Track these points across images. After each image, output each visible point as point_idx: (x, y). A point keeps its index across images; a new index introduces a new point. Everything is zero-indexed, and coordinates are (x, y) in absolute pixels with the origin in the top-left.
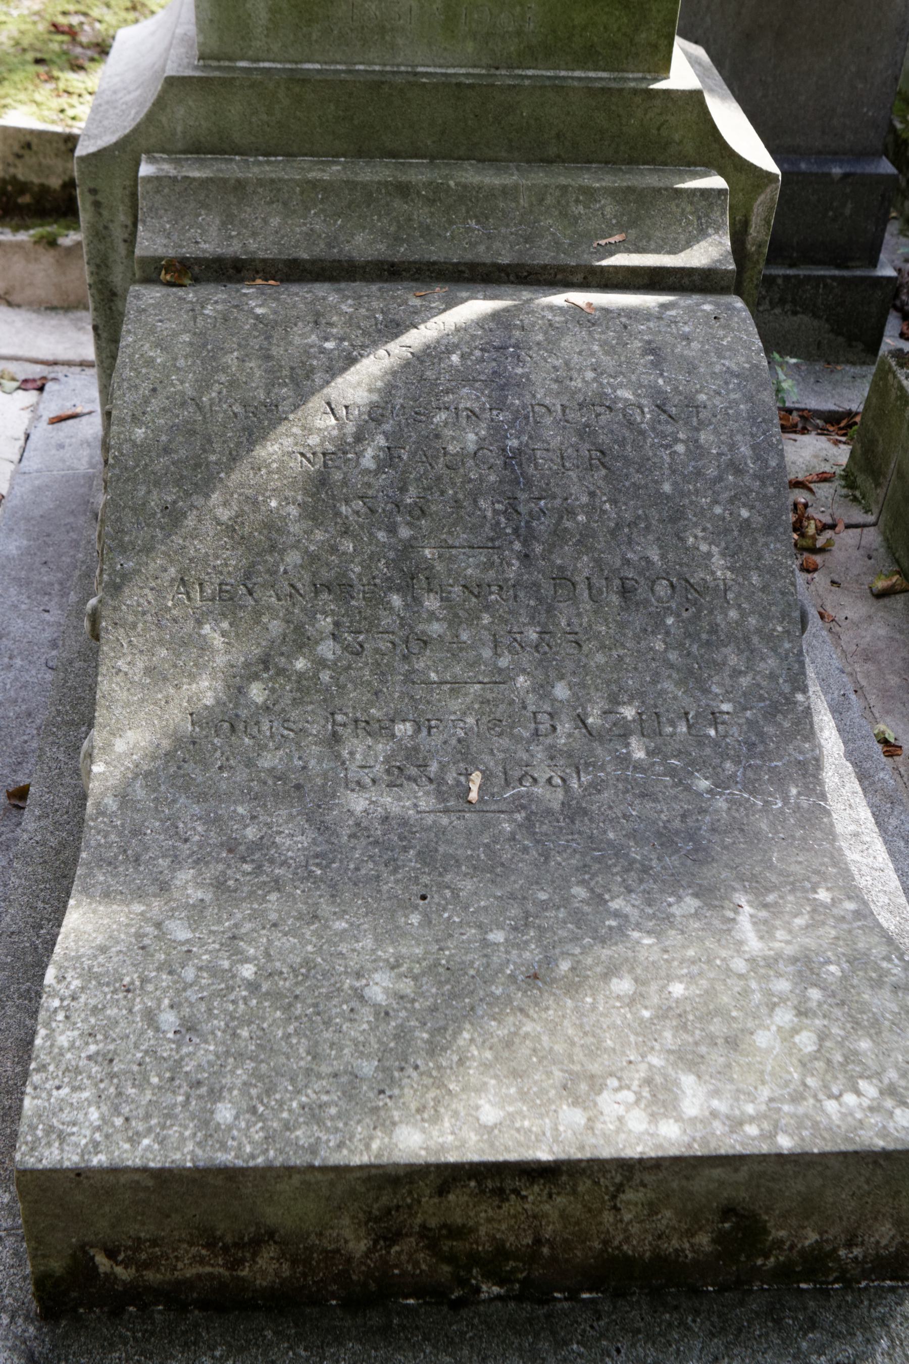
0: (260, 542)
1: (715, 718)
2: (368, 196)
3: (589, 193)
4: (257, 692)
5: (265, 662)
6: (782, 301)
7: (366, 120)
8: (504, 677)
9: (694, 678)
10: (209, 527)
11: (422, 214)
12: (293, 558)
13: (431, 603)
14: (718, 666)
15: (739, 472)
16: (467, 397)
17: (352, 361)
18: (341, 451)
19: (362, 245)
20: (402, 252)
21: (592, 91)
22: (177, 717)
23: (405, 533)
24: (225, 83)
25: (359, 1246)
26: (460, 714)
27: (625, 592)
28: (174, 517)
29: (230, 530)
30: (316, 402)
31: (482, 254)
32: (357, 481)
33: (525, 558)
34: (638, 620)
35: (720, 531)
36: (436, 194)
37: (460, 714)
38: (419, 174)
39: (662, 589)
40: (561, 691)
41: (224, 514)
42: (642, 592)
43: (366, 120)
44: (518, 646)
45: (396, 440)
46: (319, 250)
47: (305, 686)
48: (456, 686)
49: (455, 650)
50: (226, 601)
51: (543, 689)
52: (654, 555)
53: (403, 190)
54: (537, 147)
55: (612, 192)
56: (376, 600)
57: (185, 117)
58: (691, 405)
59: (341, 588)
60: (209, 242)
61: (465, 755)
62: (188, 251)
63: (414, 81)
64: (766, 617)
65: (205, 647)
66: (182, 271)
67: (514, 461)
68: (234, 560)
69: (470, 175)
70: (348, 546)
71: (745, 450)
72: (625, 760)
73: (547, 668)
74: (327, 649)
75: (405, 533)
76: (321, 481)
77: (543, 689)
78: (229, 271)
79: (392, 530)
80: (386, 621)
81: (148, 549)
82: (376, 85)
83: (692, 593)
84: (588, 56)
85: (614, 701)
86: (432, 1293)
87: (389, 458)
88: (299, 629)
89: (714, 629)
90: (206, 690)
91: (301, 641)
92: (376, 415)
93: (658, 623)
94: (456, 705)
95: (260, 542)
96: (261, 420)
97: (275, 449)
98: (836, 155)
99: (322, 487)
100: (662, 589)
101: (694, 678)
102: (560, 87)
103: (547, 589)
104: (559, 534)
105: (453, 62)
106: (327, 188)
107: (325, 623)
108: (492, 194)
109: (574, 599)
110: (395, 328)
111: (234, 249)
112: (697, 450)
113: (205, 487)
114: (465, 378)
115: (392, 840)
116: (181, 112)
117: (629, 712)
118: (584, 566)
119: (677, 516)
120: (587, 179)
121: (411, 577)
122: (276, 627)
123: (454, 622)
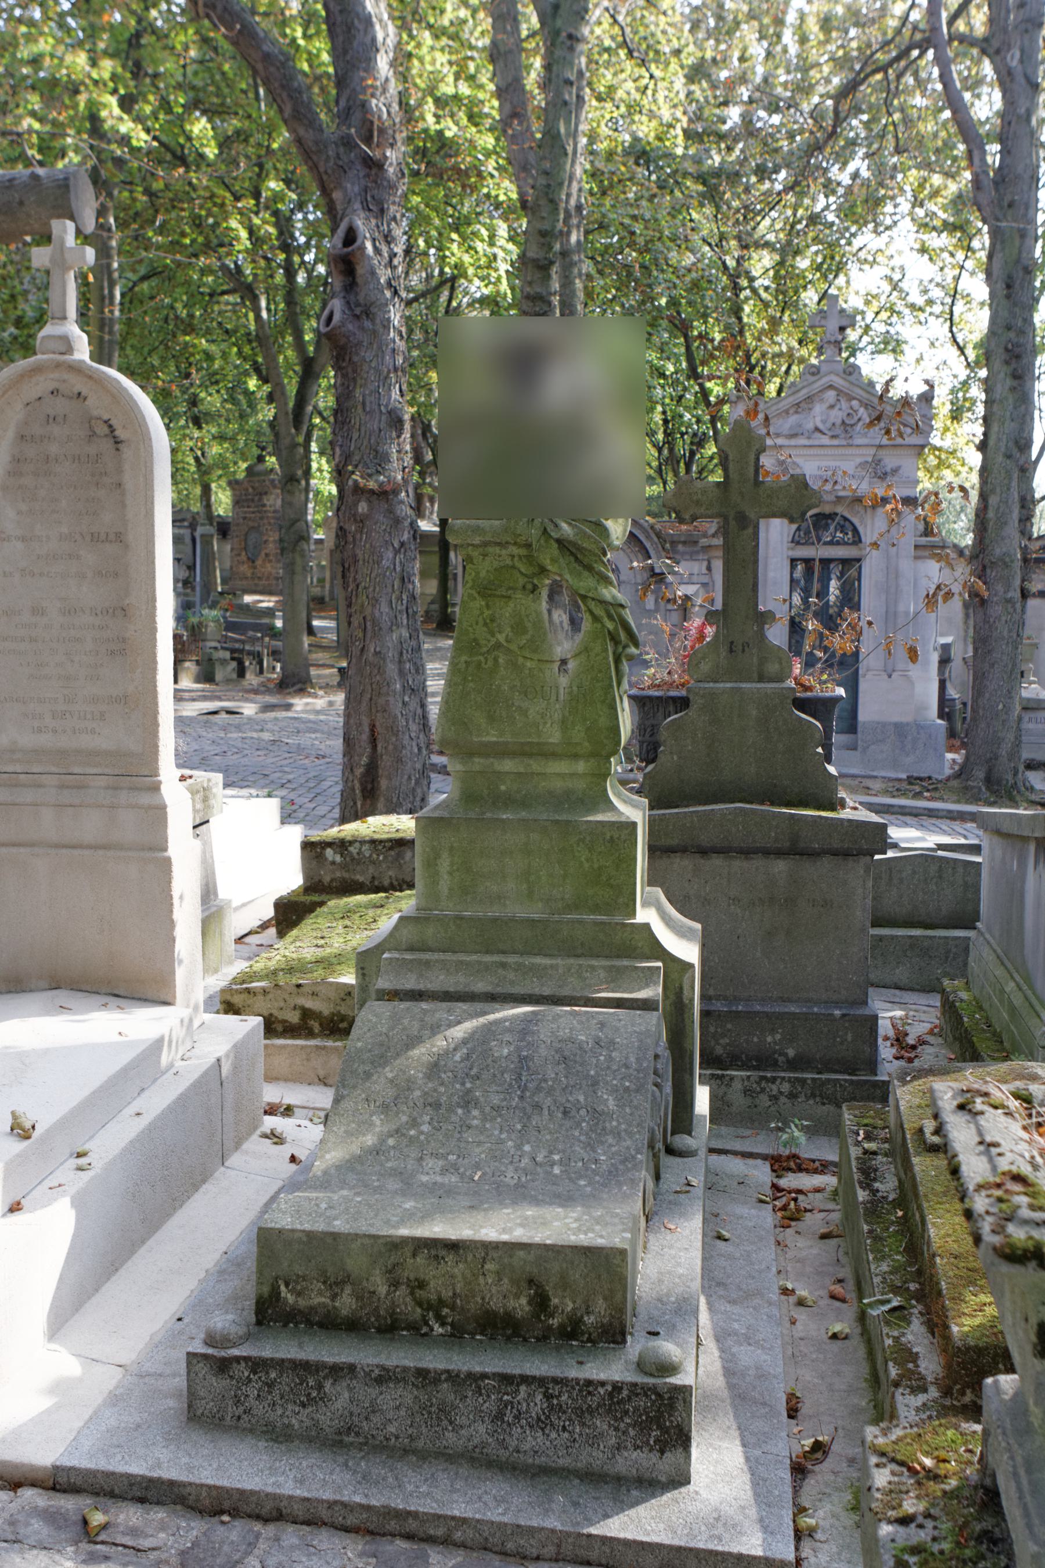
0: (403, 1088)
1: (596, 1161)
2: (487, 968)
3: (593, 968)
4: (391, 1142)
5: (397, 1131)
6: (813, 1095)
7: (491, 936)
8: (501, 1142)
9: (590, 1146)
10: (382, 1080)
11: (511, 976)
12: (417, 1093)
13: (475, 1113)
14: (602, 1143)
15: (627, 1067)
16: (508, 1037)
17: (459, 1023)
18: (447, 1053)
19: (481, 986)
20: (499, 990)
21: (596, 923)
22: (355, 1148)
23: (468, 1085)
24: (427, 919)
25: (383, 1290)
26: (479, 1153)
27: (565, 1113)
28: (368, 1075)
29: (392, 1081)
30: (440, 1036)
31: (537, 991)
32: (450, 1064)
33: (521, 1098)
34: (568, 1123)
35: (615, 1090)
36: (518, 967)
37: (479, 1153)
38: (511, 959)
39: (583, 1112)
40: (527, 1148)
41: (390, 1075)
42: (573, 1113)
43: (491, 936)
44: (511, 1130)
45: (472, 1051)
46: (460, 988)
47: (412, 1140)
48: (480, 1143)
49: (482, 1130)
50: (385, 1108)
51: (519, 1147)
52: (581, 1098)
53: (504, 965)
54: (572, 949)
55: (604, 967)
56: (451, 1110)
57: (407, 934)
58: (612, 1042)
59: (436, 1106)
60: (410, 983)
61: (477, 1166)
62: (399, 987)
63: (512, 919)
64: (630, 1125)
65: (372, 1124)
66: (394, 995)
67: (522, 1059)
68: (391, 1092)
69: (538, 960)
70: (442, 1089)
71: (632, 1059)
72: (549, 1173)
73: (523, 1136)
74: (425, 1128)
75: (468, 1085)
76: (436, 1065)
77: (519, 1147)
78: (417, 996)
79: (463, 1084)
80: (454, 1118)
81: (354, 1087)
82: (495, 920)
83: (597, 1115)
84: (596, 909)
85: (551, 1152)
86: (413, 1327)
87: (468, 1057)
88: (414, 1120)
89: (604, 1129)
90: (370, 1140)
91: (414, 1123)
92: (465, 1042)
93: (578, 1125)
94: (477, 1150)
95: (403, 1088)
96: (414, 1041)
97: (416, 1052)
98: (837, 1004)
99: (434, 1069)
100: (583, 1112)
101: (590, 1146)
102: (580, 922)
103: (529, 1110)
104: (539, 1089)
105: (535, 911)
106: (468, 964)
107: (427, 1118)
108: (545, 968)
109: (541, 1114)
110: (484, 1013)
111: (421, 987)
112: (610, 1059)
113: (384, 1065)
114: (509, 1030)
115: (432, 1188)
116: (405, 932)
117: (556, 1157)
118: (549, 1101)
119: (595, 1084)
120: (594, 962)
121: (467, 1101)
122: (404, 1118)
123: (484, 1119)
